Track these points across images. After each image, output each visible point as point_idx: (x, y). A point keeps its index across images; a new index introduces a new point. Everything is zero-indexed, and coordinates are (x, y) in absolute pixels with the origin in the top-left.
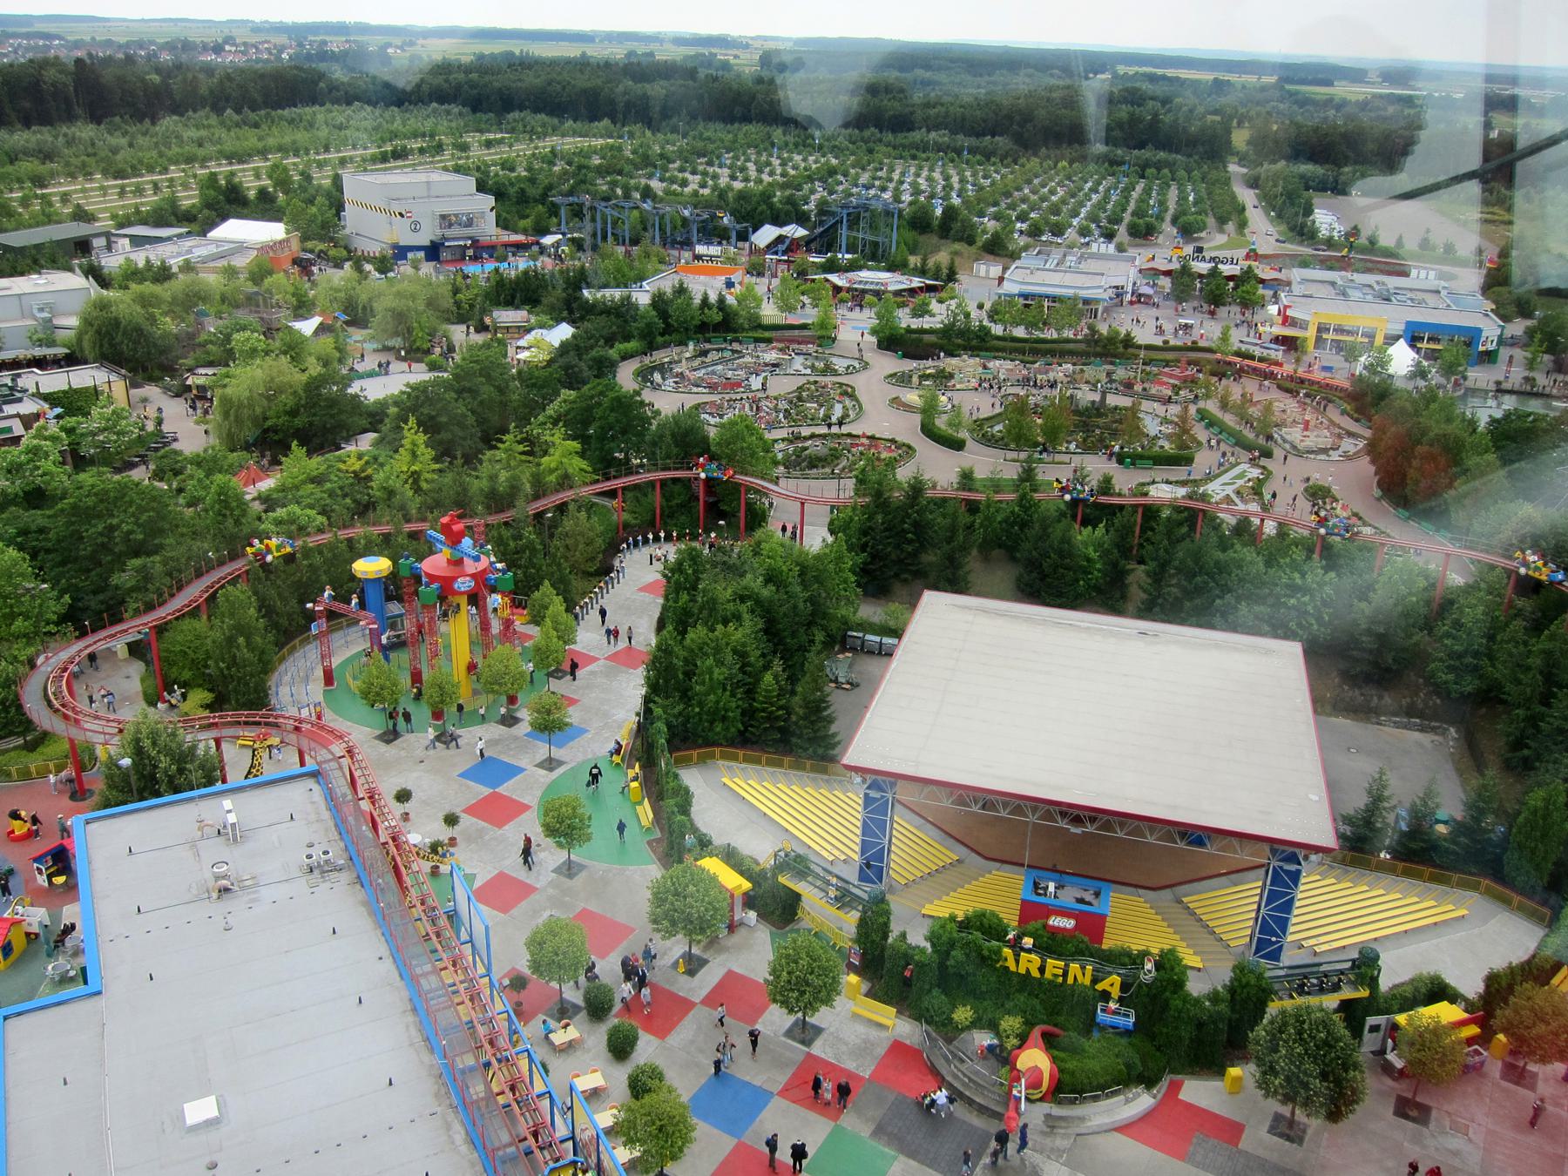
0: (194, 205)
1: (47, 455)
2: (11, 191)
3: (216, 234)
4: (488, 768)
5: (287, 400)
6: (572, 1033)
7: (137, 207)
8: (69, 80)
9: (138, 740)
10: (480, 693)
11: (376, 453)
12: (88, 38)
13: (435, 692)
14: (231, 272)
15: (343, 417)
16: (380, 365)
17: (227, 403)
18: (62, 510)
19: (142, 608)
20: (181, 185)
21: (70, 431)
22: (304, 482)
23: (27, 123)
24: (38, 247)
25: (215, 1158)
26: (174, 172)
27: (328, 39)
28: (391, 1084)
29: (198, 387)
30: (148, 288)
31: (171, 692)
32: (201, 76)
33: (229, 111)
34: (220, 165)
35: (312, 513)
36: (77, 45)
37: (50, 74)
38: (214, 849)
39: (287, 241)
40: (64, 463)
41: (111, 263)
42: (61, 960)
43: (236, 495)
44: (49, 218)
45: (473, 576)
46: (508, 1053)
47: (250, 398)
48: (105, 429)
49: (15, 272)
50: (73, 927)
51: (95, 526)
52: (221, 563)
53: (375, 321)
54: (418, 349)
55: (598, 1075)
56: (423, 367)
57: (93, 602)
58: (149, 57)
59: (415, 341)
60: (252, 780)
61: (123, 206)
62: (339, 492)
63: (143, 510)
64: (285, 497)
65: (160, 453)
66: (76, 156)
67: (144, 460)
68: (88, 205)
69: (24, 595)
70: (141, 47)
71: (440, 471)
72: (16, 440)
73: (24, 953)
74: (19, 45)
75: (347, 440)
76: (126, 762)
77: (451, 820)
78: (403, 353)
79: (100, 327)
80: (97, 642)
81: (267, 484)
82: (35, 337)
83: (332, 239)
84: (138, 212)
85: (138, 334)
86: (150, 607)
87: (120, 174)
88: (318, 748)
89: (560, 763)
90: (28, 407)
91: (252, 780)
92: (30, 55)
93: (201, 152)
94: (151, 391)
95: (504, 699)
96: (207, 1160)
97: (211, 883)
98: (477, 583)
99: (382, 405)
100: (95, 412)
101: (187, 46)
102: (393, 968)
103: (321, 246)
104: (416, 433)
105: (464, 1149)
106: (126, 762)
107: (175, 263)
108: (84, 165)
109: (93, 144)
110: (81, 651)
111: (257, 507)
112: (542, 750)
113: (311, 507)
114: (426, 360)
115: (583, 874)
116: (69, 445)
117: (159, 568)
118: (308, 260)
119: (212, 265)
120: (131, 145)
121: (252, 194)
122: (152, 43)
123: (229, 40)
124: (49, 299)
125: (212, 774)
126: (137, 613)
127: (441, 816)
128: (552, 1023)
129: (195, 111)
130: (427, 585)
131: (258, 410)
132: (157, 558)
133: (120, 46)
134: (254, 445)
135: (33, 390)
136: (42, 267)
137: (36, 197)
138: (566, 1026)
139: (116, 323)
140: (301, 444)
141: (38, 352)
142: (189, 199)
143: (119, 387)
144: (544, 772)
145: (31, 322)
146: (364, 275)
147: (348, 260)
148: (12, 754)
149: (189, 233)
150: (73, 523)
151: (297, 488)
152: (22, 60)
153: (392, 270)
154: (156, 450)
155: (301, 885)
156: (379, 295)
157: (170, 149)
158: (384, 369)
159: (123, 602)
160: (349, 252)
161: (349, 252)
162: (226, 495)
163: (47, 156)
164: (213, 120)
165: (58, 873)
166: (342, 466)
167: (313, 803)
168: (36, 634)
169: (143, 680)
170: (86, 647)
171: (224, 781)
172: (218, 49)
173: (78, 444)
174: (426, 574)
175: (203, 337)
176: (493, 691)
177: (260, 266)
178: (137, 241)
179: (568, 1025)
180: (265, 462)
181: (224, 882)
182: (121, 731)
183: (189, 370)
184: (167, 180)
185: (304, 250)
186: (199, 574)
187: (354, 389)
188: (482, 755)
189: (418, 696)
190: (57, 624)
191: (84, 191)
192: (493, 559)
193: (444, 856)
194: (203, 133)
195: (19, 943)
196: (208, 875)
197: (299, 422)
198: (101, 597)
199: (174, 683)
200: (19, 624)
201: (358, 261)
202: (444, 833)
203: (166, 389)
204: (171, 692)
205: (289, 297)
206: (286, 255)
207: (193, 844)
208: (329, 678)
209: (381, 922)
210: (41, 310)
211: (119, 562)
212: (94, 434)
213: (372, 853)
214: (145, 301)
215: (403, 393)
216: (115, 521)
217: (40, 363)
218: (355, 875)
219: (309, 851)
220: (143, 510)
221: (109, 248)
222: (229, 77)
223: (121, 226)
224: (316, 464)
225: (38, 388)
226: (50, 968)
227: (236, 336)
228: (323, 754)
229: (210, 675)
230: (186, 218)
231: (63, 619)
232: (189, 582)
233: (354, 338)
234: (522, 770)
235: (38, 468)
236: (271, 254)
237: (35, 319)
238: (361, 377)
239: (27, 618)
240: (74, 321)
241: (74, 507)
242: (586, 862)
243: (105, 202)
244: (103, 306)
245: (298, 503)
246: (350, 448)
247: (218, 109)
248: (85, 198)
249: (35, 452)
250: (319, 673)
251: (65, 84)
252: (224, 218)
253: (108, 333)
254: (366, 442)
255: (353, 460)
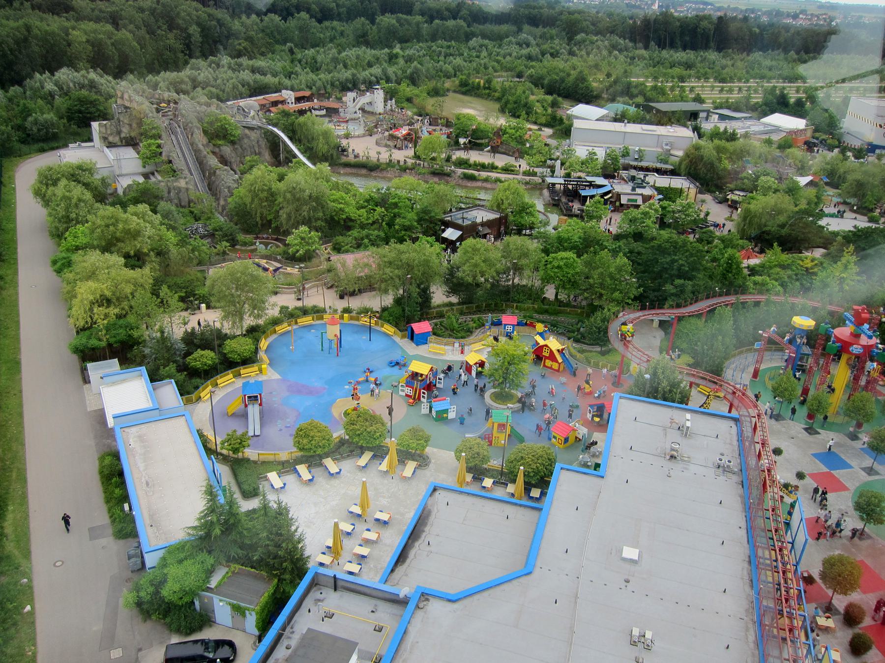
0: (757, 103)
1: (650, 217)
2: (667, 82)
3: (766, 120)
4: (829, 457)
5: (782, 219)
6: (830, 623)
7: (728, 98)
8: (712, 27)
9: (656, 368)
10: (840, 415)
11: (823, 260)
12: (726, 6)
13: (815, 403)
14: (769, 142)
15: (810, 236)
16: (839, 212)
17: (747, 212)
18: (653, 246)
19: (675, 305)
20: (754, 90)
21: (663, 208)
22: (776, 266)
23: (684, 48)
24: (673, 112)
25: (630, 578)
26: (752, 83)
27: (864, 15)
28: (725, 592)
29: (732, 201)
30: (723, 143)
31: (674, 351)
32: (783, 32)
33: (792, 52)
34: (778, 82)
35: (776, 283)
36: (719, 9)
37: (704, 24)
38: (675, 435)
39: (805, 130)
40: (655, 223)
41: (707, 127)
42: (586, 455)
43: (737, 262)
44: (682, 99)
45: (864, 347)
46: (794, 612)
47: (761, 214)
48: (680, 211)
49: (659, 123)
50: (596, 443)
51: (666, 258)
52: (720, 295)
53: (844, 186)
54: (866, 207)
55: (838, 654)
56: (866, 218)
57: (652, 295)
58: (756, 18)
59: (865, 202)
60: (702, 409)
61: (720, 98)
62: (794, 277)
63: (692, 255)
64: (763, 271)
65: (704, 230)
66: (704, 68)
67: (694, 231)
68: (703, 94)
69: (623, 281)
70: (753, 13)
71: (859, 281)
72: (637, 207)
73: (572, 445)
74: (691, 7)
75: (807, 249)
76: (647, 376)
77: (800, 476)
78: (855, 208)
79: (692, 159)
80: (647, 315)
81: (754, 261)
82: (660, 158)
83: (831, 134)
84: (727, 102)
85: (711, 166)
86: (679, 306)
87: (723, 81)
88: (743, 407)
89: (877, 473)
90: (647, 192)
91: (702, 409)
92: (694, 13)
93: (770, 74)
94: (708, 197)
95: (854, 422)
96: (626, 577)
97: (668, 451)
98: (865, 351)
99: (835, 234)
100: (678, 201)
101: (779, 13)
102: (745, 536)
103: (824, 137)
104: (852, 255)
105: (752, 645)
106: (647, 376)
107: (740, 132)
108: (706, 73)
109: (714, 63)
110: (640, 316)
111: (746, 272)
112: (868, 462)
113: (776, 280)
114: (870, 215)
115: (869, 542)
116: (661, 215)
117: (690, 288)
118: (814, 143)
119: (759, 136)
120: (733, 65)
121: (792, 101)
122: (759, 10)
123: (803, 12)
124: (671, 140)
125: (684, 399)
126: (672, 307)
127: (795, 473)
128: (821, 613)
129: (773, 50)
130: (834, 342)
131: (763, 220)
132: (690, 283)
133: (742, 11)
134: (753, 238)
135: (652, 183)
136: (673, 123)
137: (678, 87)
138: (828, 617)
139: (701, 158)
140: (779, 245)
141: (659, 165)
142: (757, 98)
143: (693, 191)
144: (863, 473)
145: (660, 150)
146: (846, 158)
147: (837, 147)
148: (594, 354)
149: (750, 118)
150: (656, 254)
151: (771, 268)
152: (690, 15)
153: (863, 158)
154: (702, 228)
155: (711, 472)
156: (853, 171)
157: (753, 70)
158: (840, 214)
159: (666, 299)
160: (840, 143)
161: (840, 143)
162: (732, 261)
163: (688, 66)
164: (782, 56)
165: (597, 416)
166: (801, 263)
167: (731, 434)
168: (622, 301)
169: (661, 341)
170: (644, 315)
171: (687, 404)
172: (795, 16)
173: (665, 215)
174: (835, 336)
175: (744, 175)
176: (849, 416)
177: (786, 141)
178: (722, 117)
179: (830, 617)
180: (757, 249)
181: (675, 453)
182: (648, 361)
183: (730, 191)
184: (746, 87)
185: (813, 137)
186: (708, 298)
187: (822, 222)
188: (830, 449)
189: (803, 403)
190: (633, 300)
191: (702, 87)
192: (878, 341)
193: (791, 492)
194: (774, 63)
195: (572, 440)
196: (668, 447)
197: (784, 232)
198: (656, 294)
199: (677, 348)
200: (617, 295)
201: (844, 150)
202: (794, 481)
203: (715, 198)
204: (674, 351)
205: (797, 162)
206: (802, 138)
207: (665, 429)
208: (756, 374)
209: (747, 510)
210: (667, 145)
211: (672, 279)
212: (674, 212)
213: (753, 474)
214: (719, 150)
215: (850, 231)
216: (676, 258)
217: (658, 171)
218: (741, 480)
219: (721, 457)
220: (692, 255)
221: (707, 119)
222: (798, 33)
223: (716, 108)
224: (785, 257)
225: (655, 183)
226: (581, 456)
227: (762, 178)
228: (744, 412)
229: (697, 350)
230: (753, 108)
231: (635, 299)
232: (702, 300)
233: (828, 193)
234: (851, 467)
235: (644, 223)
236: (794, 137)
237: (662, 148)
238: (827, 216)
239: (621, 293)
240: (680, 153)
241: (660, 246)
242: (873, 535)
243: (711, 94)
244: (697, 148)
245: (769, 276)
246: (808, 254)
247: (786, 50)
248: (702, 91)
249: (646, 214)
250: (751, 370)
251: (710, 30)
252: (773, 112)
253: (695, 162)
254: (818, 253)
255: (808, 261)
